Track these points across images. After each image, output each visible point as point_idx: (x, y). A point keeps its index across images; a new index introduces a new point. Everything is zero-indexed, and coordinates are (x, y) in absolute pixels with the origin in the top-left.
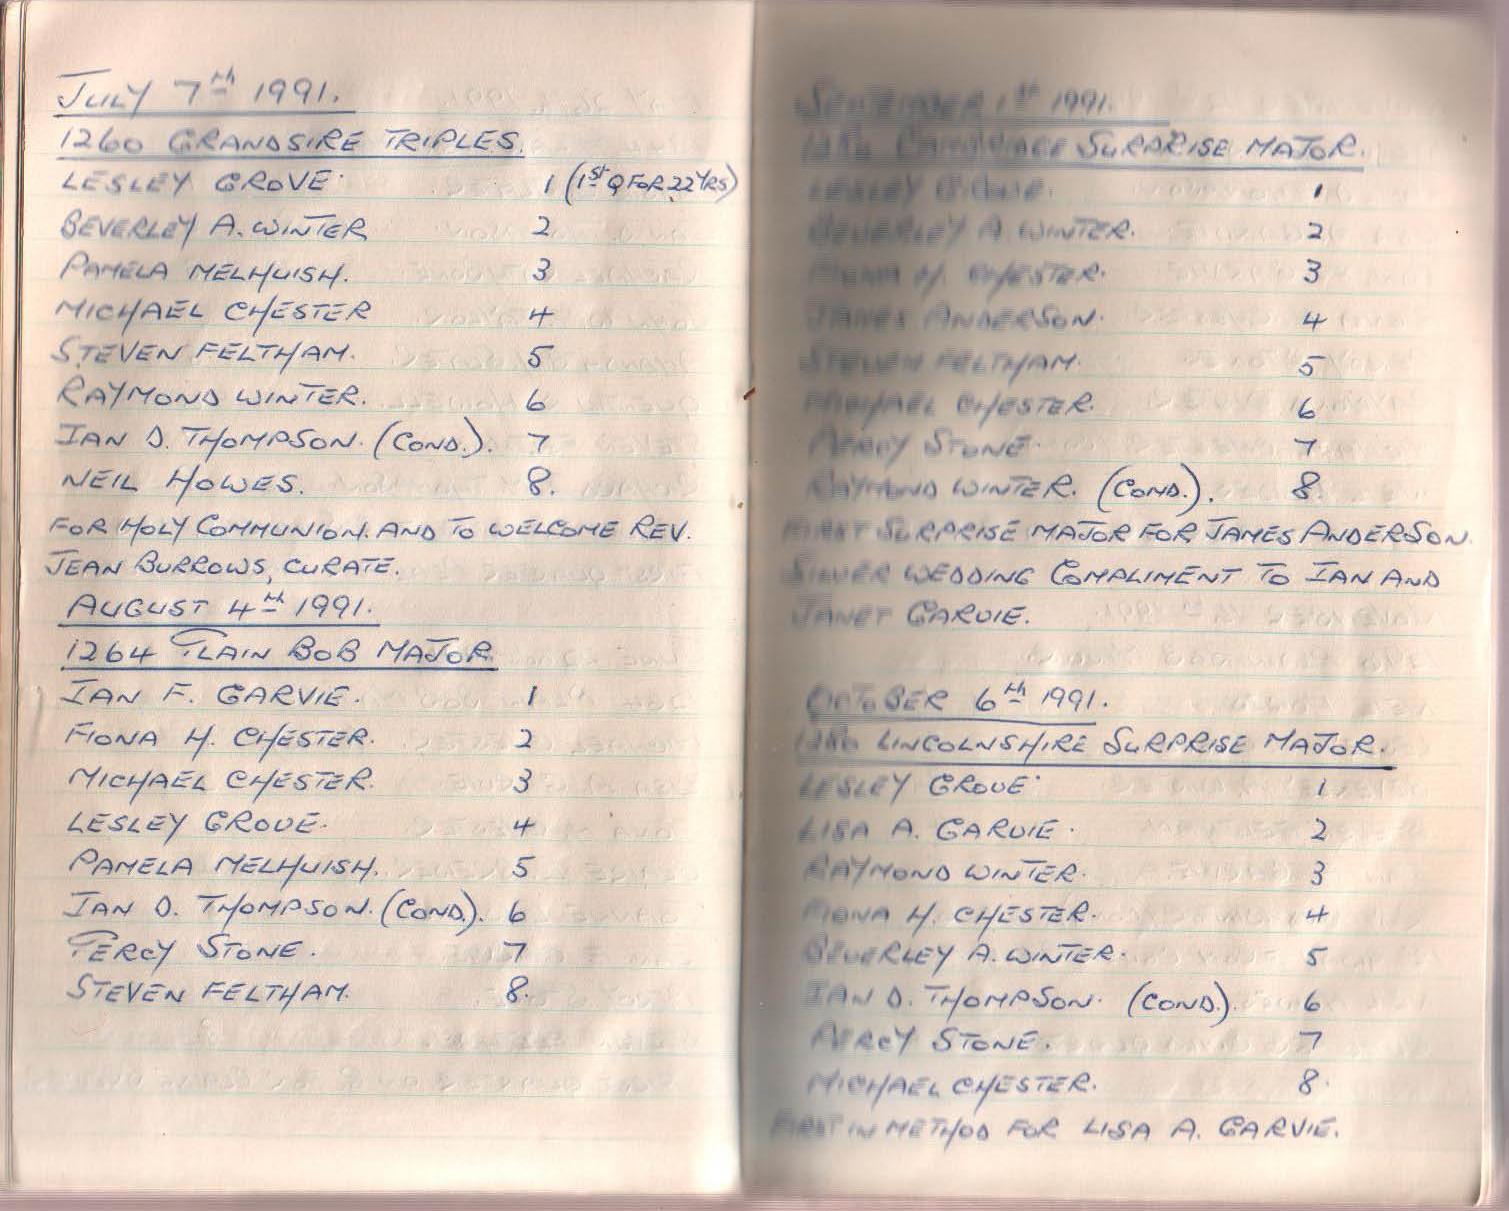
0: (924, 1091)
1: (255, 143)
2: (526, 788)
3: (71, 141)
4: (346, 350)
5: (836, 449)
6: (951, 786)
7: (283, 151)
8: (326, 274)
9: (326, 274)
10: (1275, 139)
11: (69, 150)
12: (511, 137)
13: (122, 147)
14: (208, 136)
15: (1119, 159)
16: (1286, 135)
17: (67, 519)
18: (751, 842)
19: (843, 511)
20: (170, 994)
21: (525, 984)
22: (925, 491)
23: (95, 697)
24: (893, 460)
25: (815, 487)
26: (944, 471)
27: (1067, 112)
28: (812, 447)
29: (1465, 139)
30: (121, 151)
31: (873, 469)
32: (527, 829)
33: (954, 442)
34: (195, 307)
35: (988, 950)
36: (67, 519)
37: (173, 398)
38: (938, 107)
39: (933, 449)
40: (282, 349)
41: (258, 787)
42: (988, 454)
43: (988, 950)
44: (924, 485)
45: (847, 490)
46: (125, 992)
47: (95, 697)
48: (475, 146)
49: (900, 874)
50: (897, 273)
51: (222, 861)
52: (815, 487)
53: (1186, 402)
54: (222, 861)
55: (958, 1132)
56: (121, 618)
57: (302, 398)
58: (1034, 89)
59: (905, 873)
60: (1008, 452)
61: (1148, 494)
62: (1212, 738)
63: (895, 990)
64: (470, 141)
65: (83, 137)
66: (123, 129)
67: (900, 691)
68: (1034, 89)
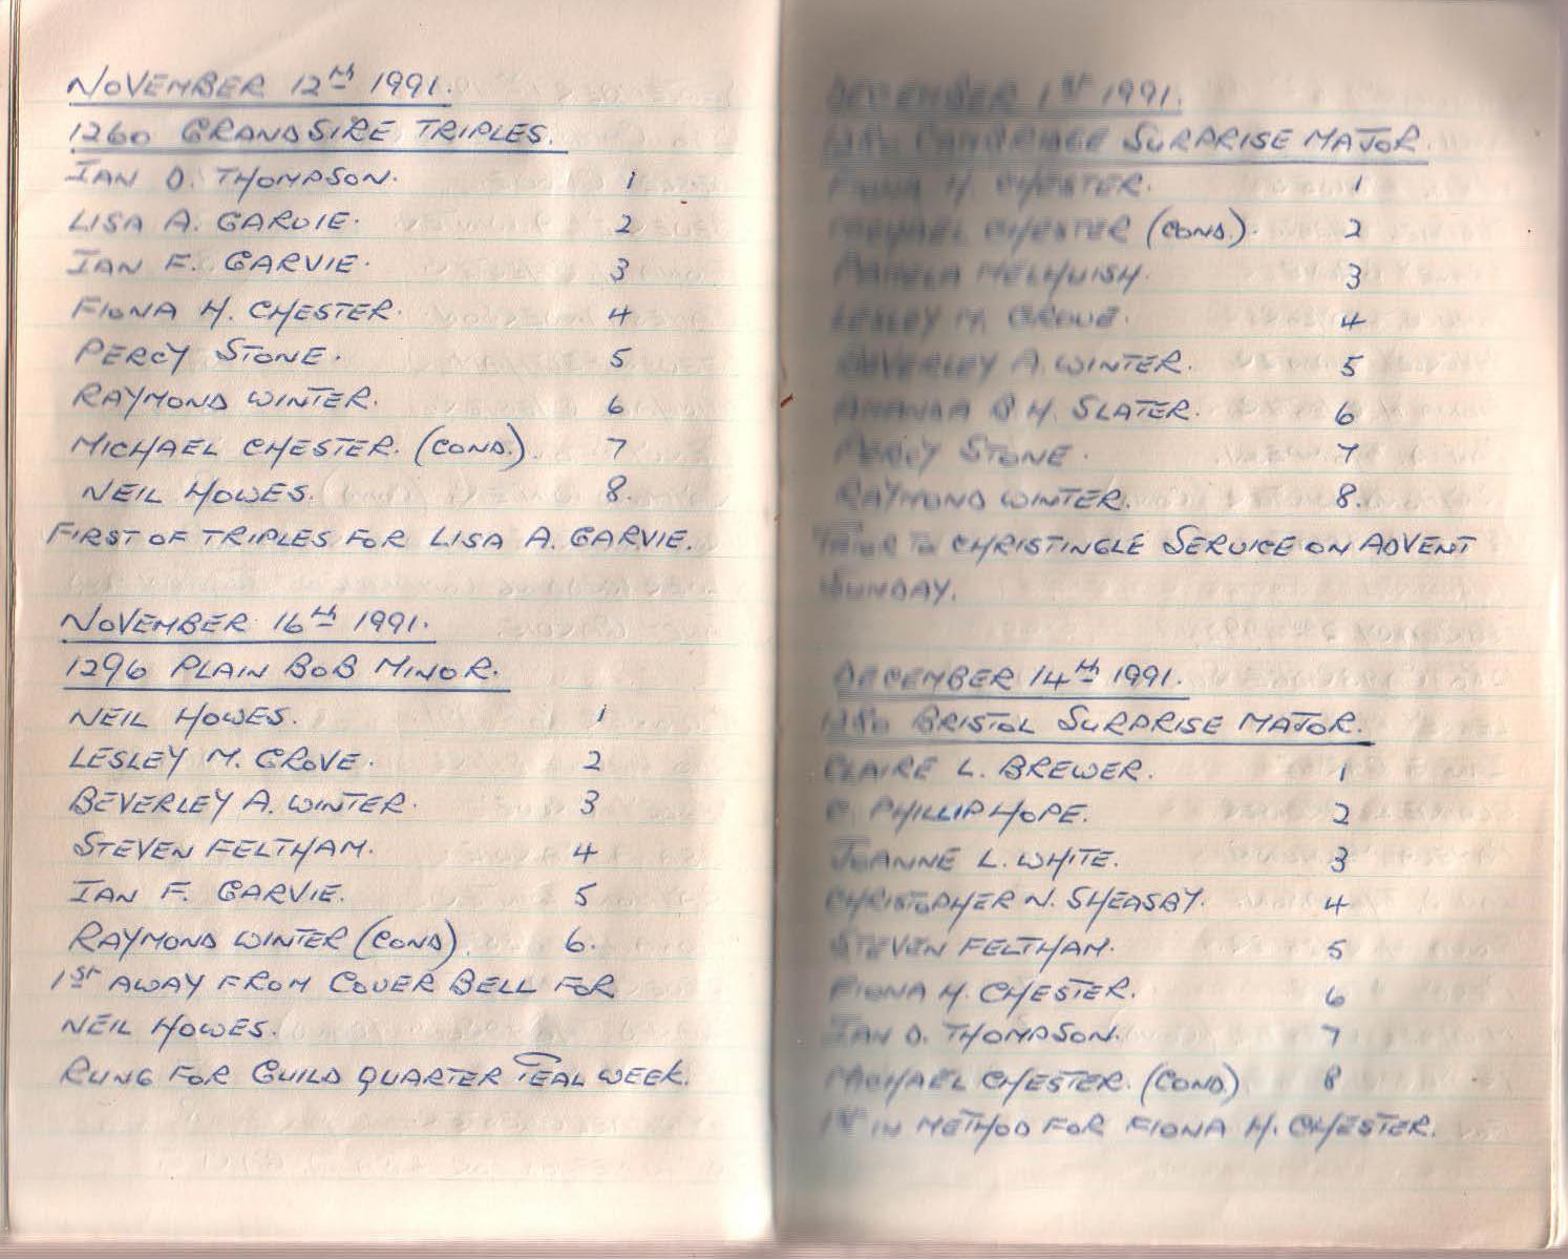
0: (198, 451)
1: (270, 135)
2: (353, 673)
3: (302, 87)
4: (363, 845)
5: (865, 457)
6: (248, 262)
7: (306, 142)
8: (212, 305)
9: (212, 305)
10: (1335, 131)
11: (78, 141)
12: (538, 131)
13: (129, 140)
14: (1179, 137)
15: (1168, 153)
16: (1346, 127)
17: (72, 524)
18: (782, 868)
19: (878, 525)
20: (177, 851)
21: (1352, 492)
22: (970, 502)
23: (100, 896)
24: (923, 467)
25: (843, 494)
26: (986, 478)
27: (1145, 104)
28: (838, 454)
29: (1538, 134)
30: (129, 144)
31: (911, 480)
32: (626, 317)
33: (992, 449)
34: (576, 1077)
35: (548, 533)
36: (72, 524)
37: (185, 402)
38: (967, 98)
39: (969, 455)
40: (298, 845)
41: (273, 454)
42: (1028, 461)
43: (548, 533)
44: (968, 496)
45: (878, 498)
46: (135, 848)
47: (100, 896)
48: (507, 139)
49: (1169, 1130)
50: (958, 275)
51: (213, 754)
52: (843, 494)
53: (1239, 407)
54: (213, 754)
55: (202, 665)
56: (130, 634)
57: (311, 400)
58: (1085, 79)
59: (891, 322)
60: (1050, 461)
61: (279, 182)
62: (1178, 719)
63: (916, 1028)
64: (502, 134)
65: (93, 131)
66: (131, 121)
67: (211, 78)
68: (1085, 79)
